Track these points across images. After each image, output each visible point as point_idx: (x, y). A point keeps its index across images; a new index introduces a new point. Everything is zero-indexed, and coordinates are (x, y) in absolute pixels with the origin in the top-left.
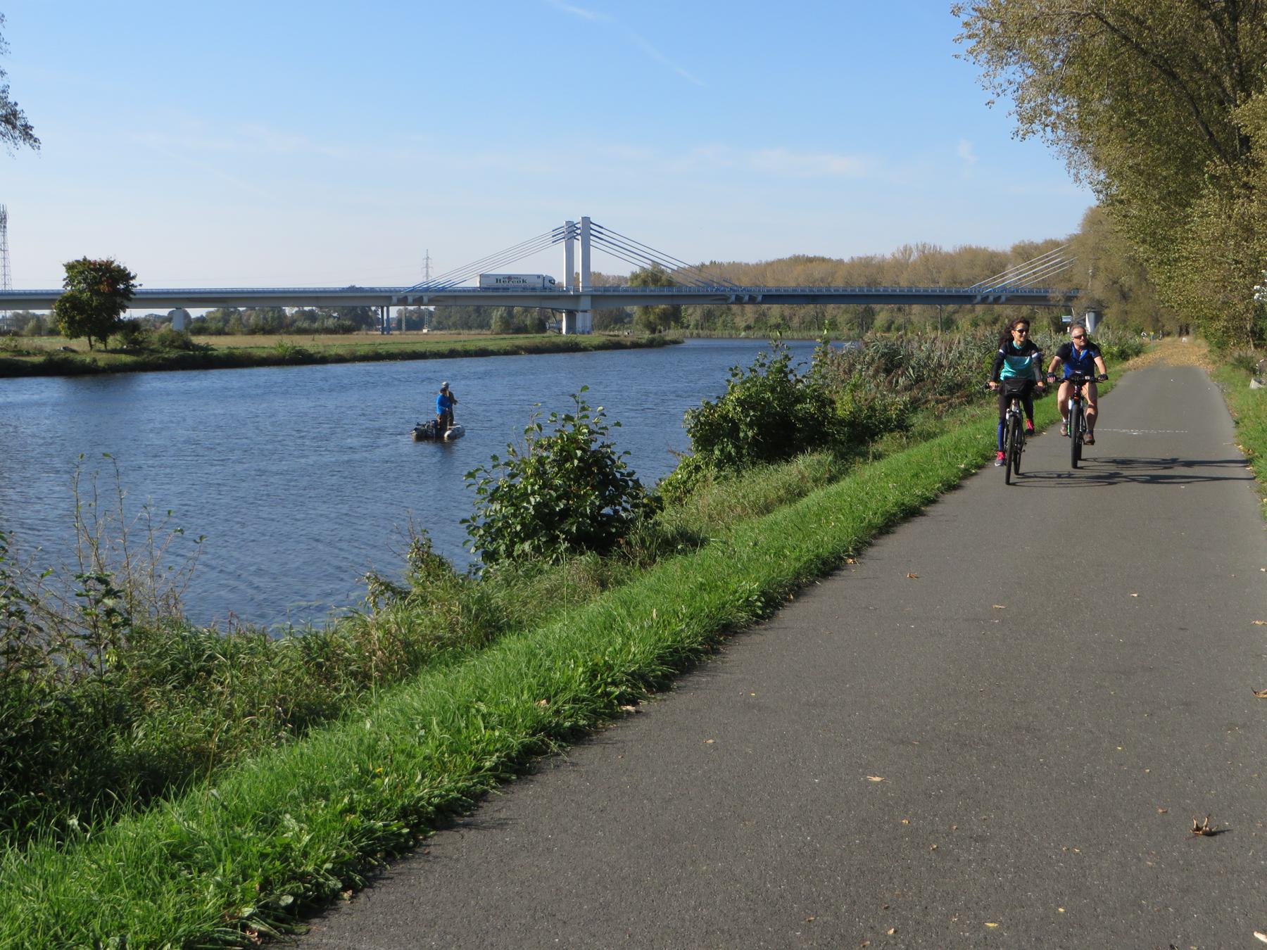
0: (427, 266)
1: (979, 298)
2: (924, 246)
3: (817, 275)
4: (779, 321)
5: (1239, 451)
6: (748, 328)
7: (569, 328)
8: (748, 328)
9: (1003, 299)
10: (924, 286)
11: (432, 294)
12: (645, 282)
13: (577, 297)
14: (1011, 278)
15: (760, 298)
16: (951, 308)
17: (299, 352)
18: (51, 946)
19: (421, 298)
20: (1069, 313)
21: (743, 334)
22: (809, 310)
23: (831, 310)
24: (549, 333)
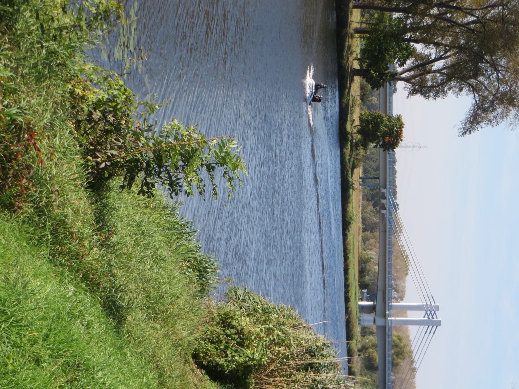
7: (362, 308)
11: (387, 216)
12: (396, 346)
13: (385, 316)
17: (350, 223)
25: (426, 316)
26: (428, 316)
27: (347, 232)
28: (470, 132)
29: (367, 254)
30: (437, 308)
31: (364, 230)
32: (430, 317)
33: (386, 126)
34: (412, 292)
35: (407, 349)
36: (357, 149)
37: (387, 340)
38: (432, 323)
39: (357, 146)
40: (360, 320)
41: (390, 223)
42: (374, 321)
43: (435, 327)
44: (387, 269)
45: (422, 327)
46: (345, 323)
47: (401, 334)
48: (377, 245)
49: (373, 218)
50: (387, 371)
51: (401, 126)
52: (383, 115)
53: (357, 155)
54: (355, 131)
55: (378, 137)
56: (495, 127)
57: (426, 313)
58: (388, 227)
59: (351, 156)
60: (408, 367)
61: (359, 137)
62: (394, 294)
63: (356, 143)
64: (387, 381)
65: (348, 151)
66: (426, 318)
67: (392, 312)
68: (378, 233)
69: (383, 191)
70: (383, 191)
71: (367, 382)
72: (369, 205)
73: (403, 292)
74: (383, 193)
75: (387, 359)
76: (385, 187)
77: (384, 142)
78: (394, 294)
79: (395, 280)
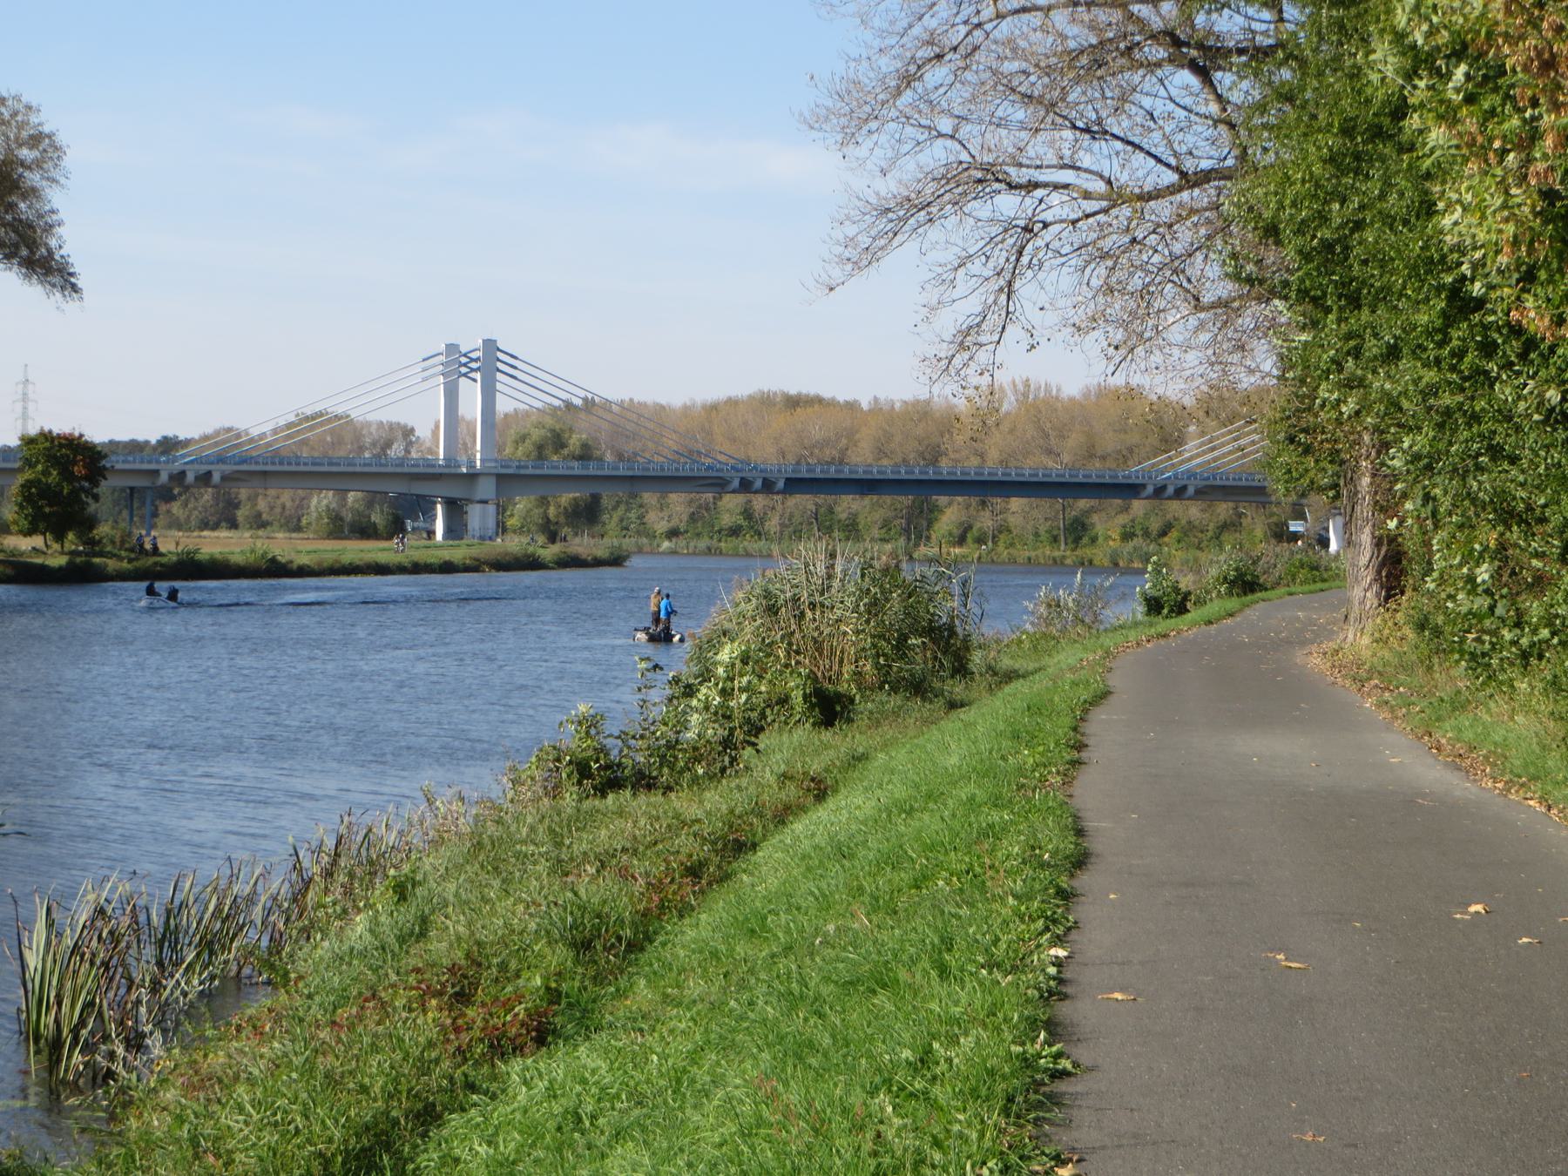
0: (25, 398)
1: (1150, 489)
2: (1027, 383)
3: (816, 433)
4: (741, 521)
5: (1170, 285)
6: (673, 533)
7: (450, 532)
8: (673, 533)
9: (1191, 490)
10: (1036, 465)
11: (228, 468)
13: (473, 477)
14: (1195, 454)
15: (781, 484)
16: (1083, 504)
17: (273, 560)
18: (316, 1167)
19: (209, 474)
20: (1300, 516)
21: (666, 544)
22: (803, 503)
23: (848, 505)
24: (411, 540)
25: (472, 375)
26: (472, 370)
27: (295, 566)
28: (71, 275)
29: (320, 517)
30: (452, 348)
31: (233, 525)
32: (474, 365)
33: (46, 473)
34: (417, 409)
35: (549, 421)
36: (100, 542)
37: (530, 471)
38: (489, 362)
39: (92, 542)
40: (482, 538)
41: (244, 461)
42: (485, 502)
43: (500, 355)
44: (358, 469)
45: (499, 386)
46: (502, 574)
47: (512, 433)
48: (272, 492)
49: (202, 502)
50: (606, 472)
51: (46, 436)
52: (21, 479)
53: (113, 542)
54: (56, 546)
55: (75, 494)
56: (62, 215)
57: (465, 375)
58: (253, 468)
59: (120, 559)
60: (582, 415)
61: (71, 536)
62: (396, 451)
63: (84, 544)
64: (630, 473)
65: (112, 565)
66: (478, 376)
67: (463, 458)
68: (243, 491)
69: (164, 477)
70: (164, 477)
71: (622, 520)
72: (168, 511)
73: (393, 427)
74: (171, 477)
75: (576, 472)
76: (156, 473)
77: (86, 478)
78: (396, 451)
79: (361, 449)
